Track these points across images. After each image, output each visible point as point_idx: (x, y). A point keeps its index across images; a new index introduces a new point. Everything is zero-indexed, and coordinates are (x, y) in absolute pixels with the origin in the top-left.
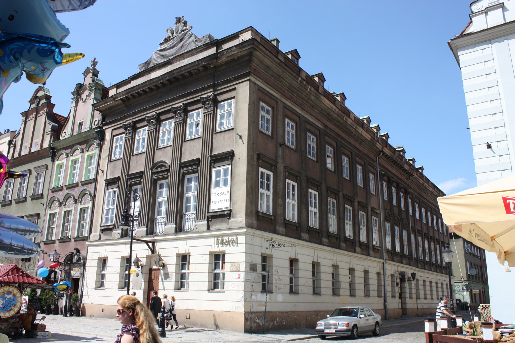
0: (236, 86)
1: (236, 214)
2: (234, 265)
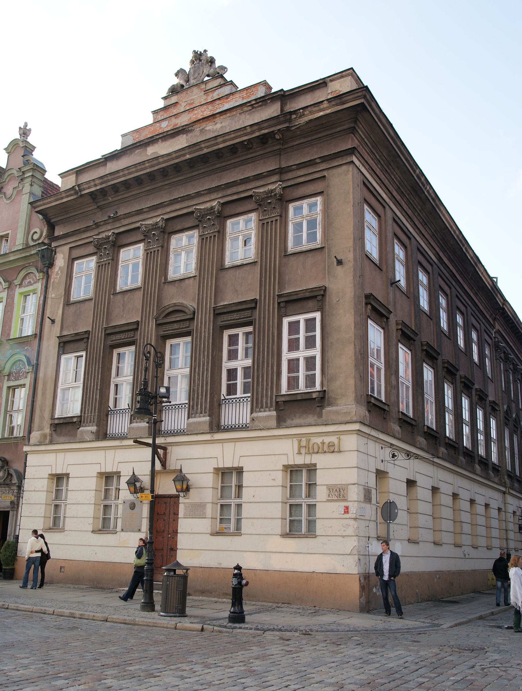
0: (325, 173)
1: (336, 399)
2: (336, 490)
